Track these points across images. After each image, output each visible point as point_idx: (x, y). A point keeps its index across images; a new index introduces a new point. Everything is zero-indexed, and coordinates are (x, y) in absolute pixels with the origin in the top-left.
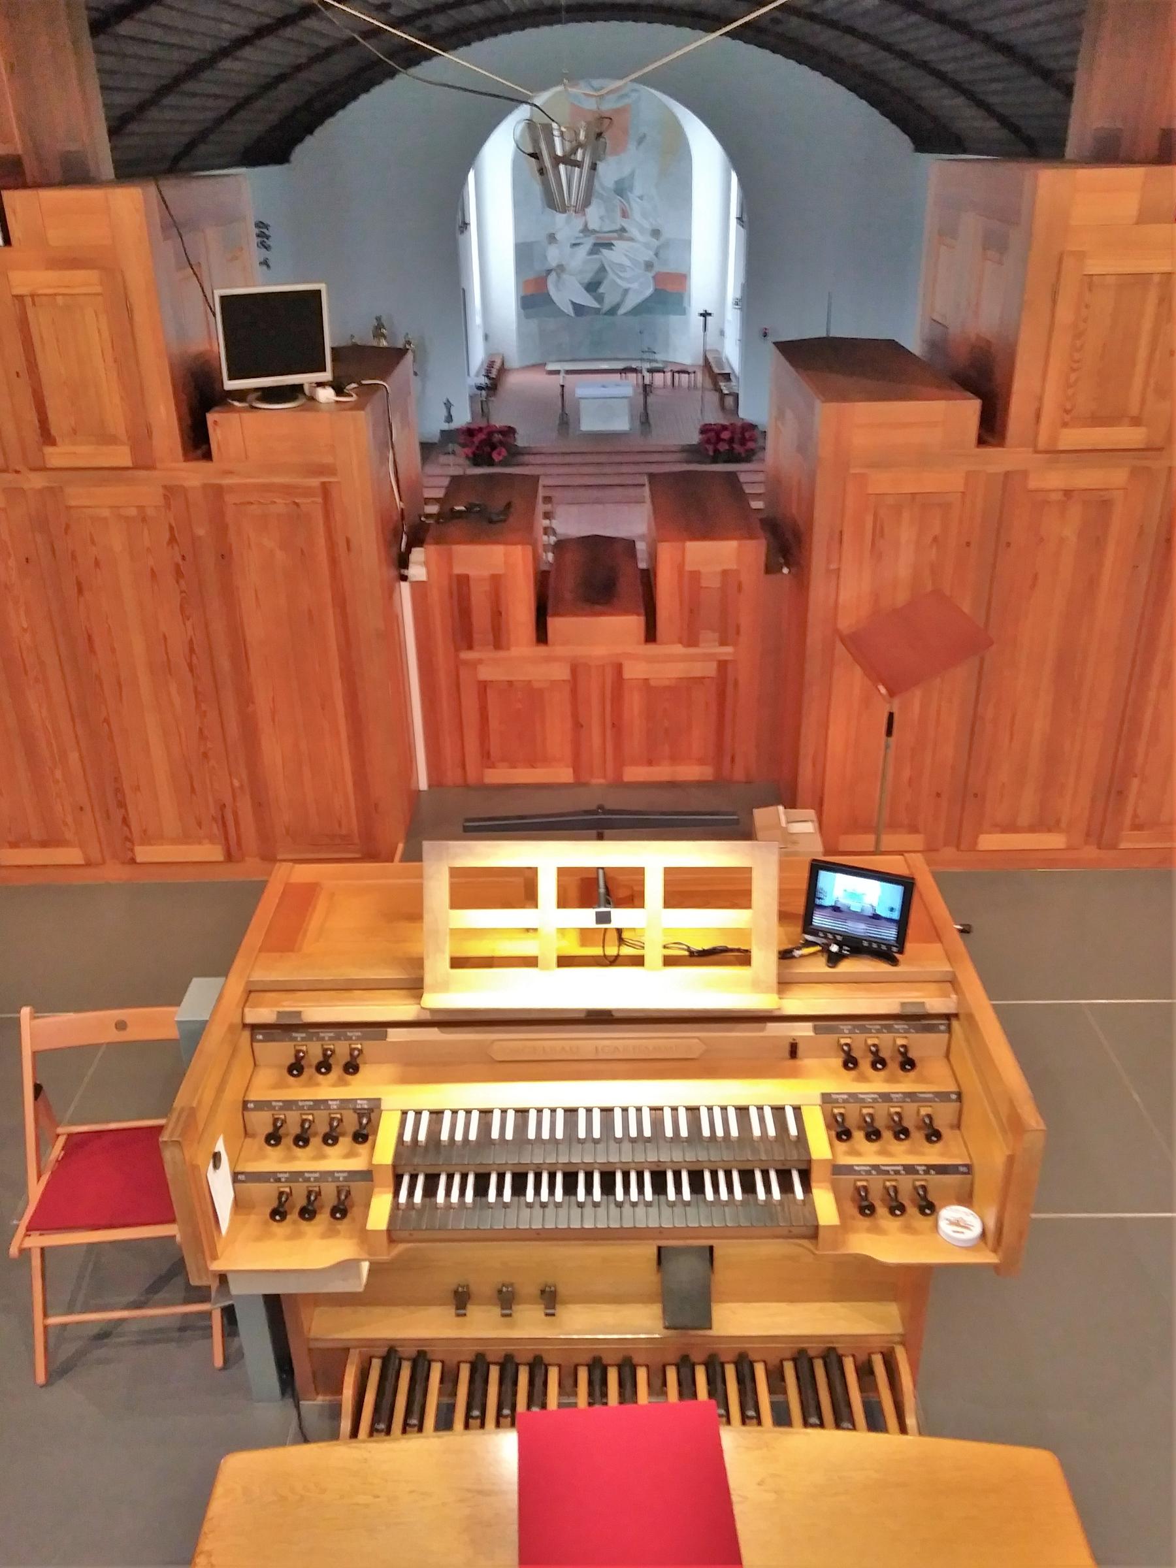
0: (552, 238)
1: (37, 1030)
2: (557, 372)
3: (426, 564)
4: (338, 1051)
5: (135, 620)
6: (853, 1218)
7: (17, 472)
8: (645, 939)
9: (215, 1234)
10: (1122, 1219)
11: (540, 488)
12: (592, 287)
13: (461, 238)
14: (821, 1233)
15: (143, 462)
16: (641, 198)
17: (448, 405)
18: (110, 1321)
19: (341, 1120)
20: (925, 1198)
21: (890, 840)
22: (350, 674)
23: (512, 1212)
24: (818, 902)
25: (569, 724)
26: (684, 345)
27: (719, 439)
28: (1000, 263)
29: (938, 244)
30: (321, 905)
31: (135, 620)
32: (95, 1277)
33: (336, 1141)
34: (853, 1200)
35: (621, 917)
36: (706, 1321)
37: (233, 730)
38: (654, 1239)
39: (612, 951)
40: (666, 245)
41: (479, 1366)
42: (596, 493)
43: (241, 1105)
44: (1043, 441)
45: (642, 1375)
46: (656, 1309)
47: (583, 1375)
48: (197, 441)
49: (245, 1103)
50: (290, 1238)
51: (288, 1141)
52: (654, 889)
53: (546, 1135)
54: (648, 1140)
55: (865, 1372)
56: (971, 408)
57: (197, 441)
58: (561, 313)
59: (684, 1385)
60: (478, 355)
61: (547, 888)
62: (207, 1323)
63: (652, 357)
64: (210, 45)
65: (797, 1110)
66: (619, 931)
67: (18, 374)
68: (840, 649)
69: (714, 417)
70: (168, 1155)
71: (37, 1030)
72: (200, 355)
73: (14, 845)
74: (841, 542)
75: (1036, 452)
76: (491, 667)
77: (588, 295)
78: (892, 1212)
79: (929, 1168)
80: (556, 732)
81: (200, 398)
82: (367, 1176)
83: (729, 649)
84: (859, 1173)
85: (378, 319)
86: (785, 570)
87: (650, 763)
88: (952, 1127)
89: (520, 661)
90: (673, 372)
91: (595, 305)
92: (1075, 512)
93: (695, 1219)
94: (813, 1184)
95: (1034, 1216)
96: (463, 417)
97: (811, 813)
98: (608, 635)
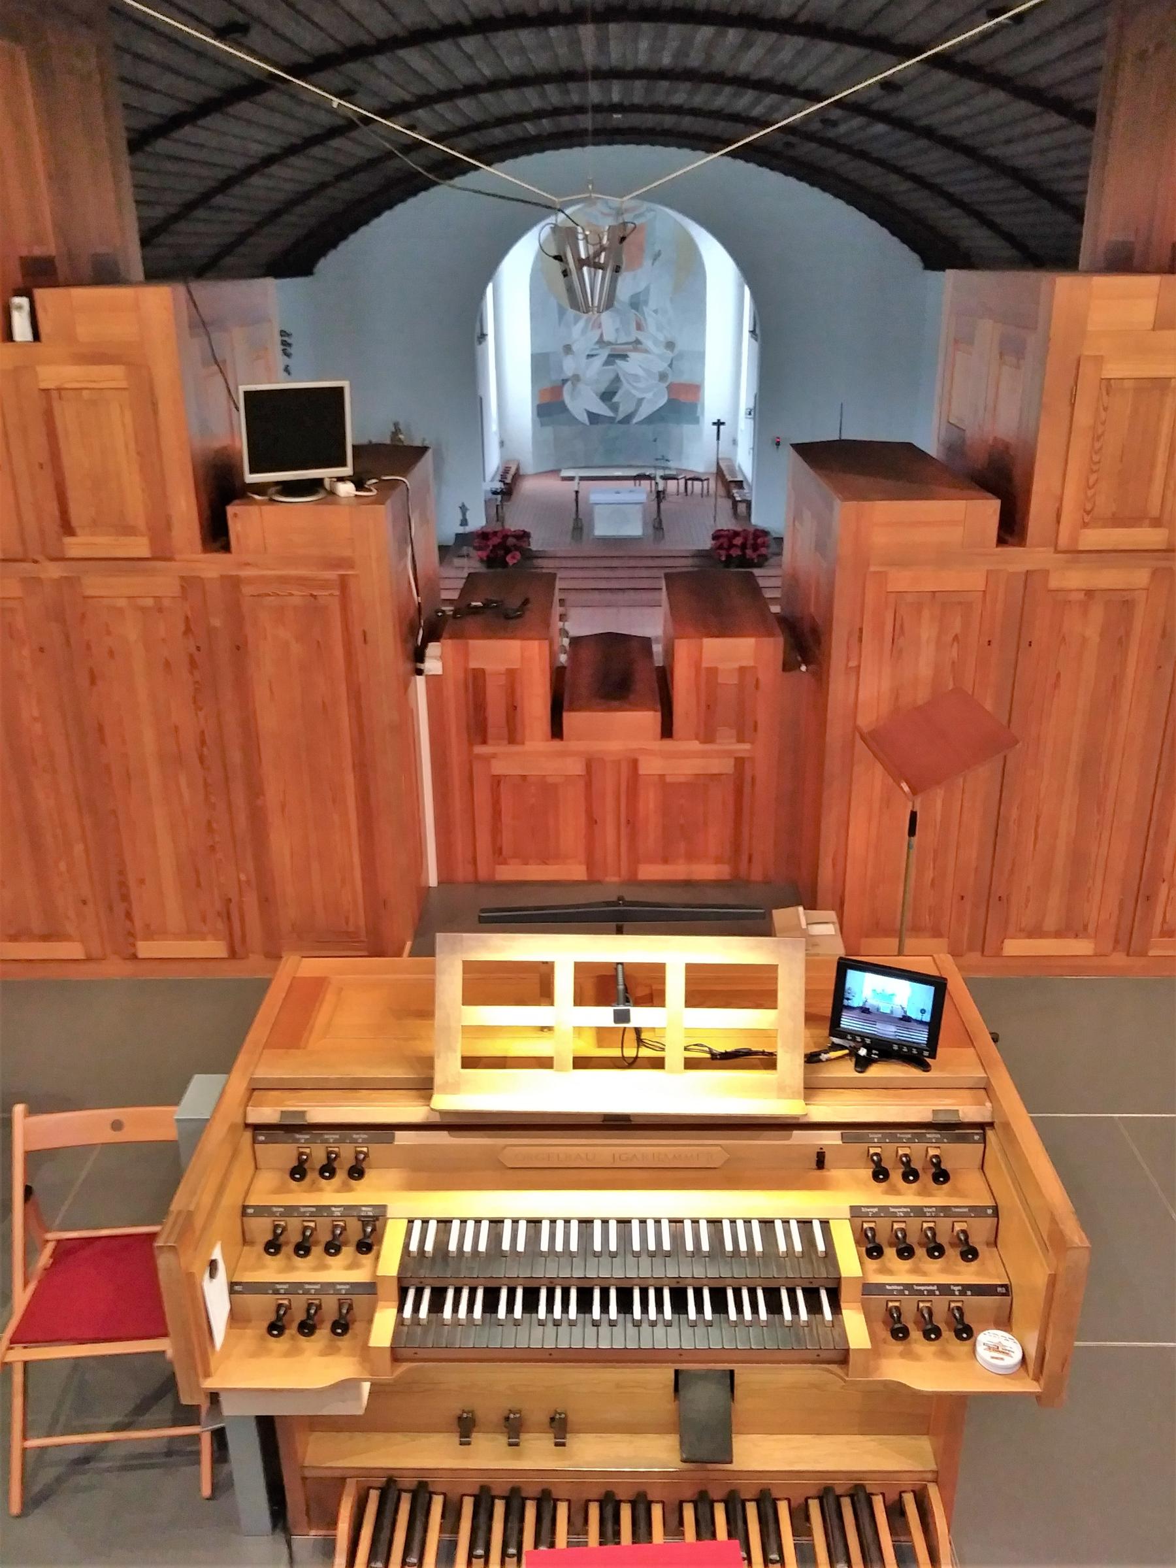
0: (568, 349)
1: (28, 1129)
2: (571, 479)
3: (442, 658)
4: (343, 1154)
5: (147, 711)
6: (885, 1341)
7: (35, 562)
8: (667, 1041)
9: (209, 1349)
10: (1164, 1348)
11: (557, 591)
12: (607, 396)
13: (479, 347)
14: (852, 1358)
15: (162, 554)
16: (656, 311)
17: (463, 509)
18: (95, 1443)
19: (344, 1229)
20: (961, 1320)
21: (910, 943)
22: (363, 768)
23: (523, 1331)
24: (846, 1002)
25: (583, 819)
26: (697, 454)
27: (731, 546)
28: (1018, 367)
29: (950, 352)
30: (329, 998)
31: (147, 711)
32: (78, 1396)
33: (338, 1251)
34: (884, 1322)
35: (640, 1016)
36: (727, 1456)
37: (242, 820)
38: (673, 1362)
39: (630, 1052)
40: (681, 356)
41: (483, 1501)
42: (608, 596)
43: (240, 1210)
44: (1064, 541)
45: (657, 1512)
46: (672, 1440)
47: (594, 1511)
48: (216, 533)
49: (245, 1207)
50: (287, 1354)
51: (288, 1250)
52: (675, 986)
53: (559, 1247)
54: (668, 1255)
55: (896, 1512)
56: (993, 506)
57: (216, 533)
58: (573, 420)
59: (703, 1525)
60: (493, 461)
61: (564, 984)
62: (194, 1448)
63: (663, 464)
64: (240, 163)
65: (825, 1223)
66: (638, 1031)
67: (41, 466)
68: (860, 745)
69: (727, 523)
70: (163, 1262)
71: (28, 1129)
72: (225, 448)
73: (14, 938)
74: (860, 640)
75: (1057, 551)
76: (505, 761)
77: (602, 404)
78: (926, 1335)
79: (965, 1289)
80: (570, 829)
81: (220, 490)
82: (370, 1288)
83: (747, 746)
84: (891, 1293)
85: (396, 425)
86: (803, 668)
87: (665, 861)
88: (988, 1244)
89: (534, 755)
90: (686, 480)
91: (610, 414)
92: (1097, 613)
93: (716, 1340)
94: (843, 1305)
95: (1077, 1344)
96: (478, 521)
97: (832, 915)
98: (625, 730)
